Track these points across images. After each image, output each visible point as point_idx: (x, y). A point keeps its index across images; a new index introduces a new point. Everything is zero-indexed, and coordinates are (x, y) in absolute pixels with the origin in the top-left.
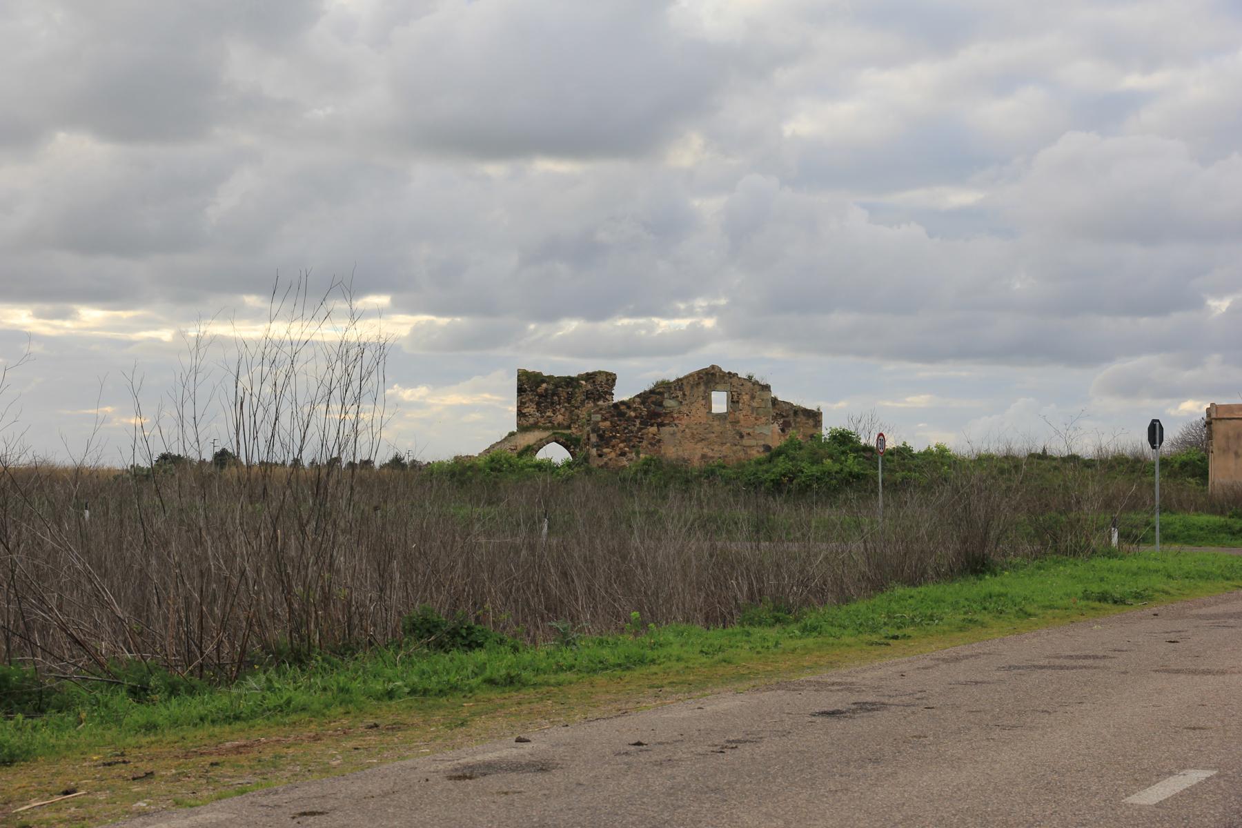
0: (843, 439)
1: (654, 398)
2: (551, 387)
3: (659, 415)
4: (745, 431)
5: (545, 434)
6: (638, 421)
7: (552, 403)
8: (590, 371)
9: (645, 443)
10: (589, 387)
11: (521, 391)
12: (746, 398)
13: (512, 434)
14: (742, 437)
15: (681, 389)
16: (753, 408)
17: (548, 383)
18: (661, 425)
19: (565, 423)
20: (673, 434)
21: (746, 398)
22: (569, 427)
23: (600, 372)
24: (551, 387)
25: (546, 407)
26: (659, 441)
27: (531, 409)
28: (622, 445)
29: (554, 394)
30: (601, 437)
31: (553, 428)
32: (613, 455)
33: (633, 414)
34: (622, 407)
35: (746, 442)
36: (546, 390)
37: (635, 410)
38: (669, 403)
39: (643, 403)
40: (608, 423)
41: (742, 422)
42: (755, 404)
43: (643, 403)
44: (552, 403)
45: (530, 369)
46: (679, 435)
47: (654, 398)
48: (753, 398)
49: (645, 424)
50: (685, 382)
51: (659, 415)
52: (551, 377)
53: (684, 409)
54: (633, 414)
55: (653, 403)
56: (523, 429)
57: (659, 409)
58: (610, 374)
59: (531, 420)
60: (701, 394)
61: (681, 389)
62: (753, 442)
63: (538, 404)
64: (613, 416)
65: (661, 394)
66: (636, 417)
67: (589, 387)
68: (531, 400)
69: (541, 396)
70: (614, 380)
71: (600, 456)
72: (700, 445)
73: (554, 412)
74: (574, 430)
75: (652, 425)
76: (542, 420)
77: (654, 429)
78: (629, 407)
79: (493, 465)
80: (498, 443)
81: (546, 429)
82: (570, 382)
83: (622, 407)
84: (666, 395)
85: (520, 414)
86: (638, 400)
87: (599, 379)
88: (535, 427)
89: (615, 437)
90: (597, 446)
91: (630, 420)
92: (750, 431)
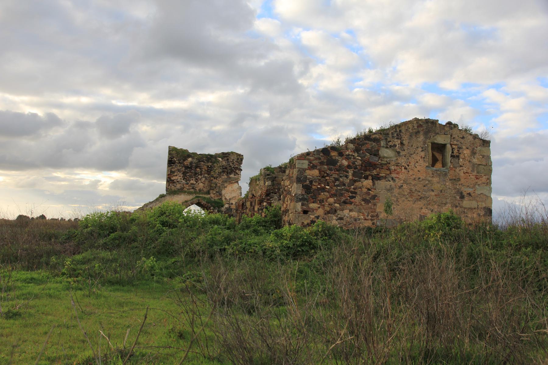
0: (70, 220)
1: (370, 145)
2: (195, 161)
3: (374, 166)
4: (466, 190)
5: (189, 197)
6: (351, 172)
7: (196, 174)
8: (226, 151)
9: (358, 199)
10: (224, 163)
11: (171, 162)
12: (467, 152)
13: (162, 196)
14: (462, 197)
15: (399, 137)
16: (474, 165)
17: (193, 158)
18: (376, 178)
19: (205, 190)
20: (390, 190)
21: (467, 152)
22: (208, 193)
23: (232, 153)
24: (195, 161)
25: (191, 177)
26: (374, 197)
27: (178, 177)
28: (331, 200)
29: (197, 167)
30: (307, 188)
31: (195, 192)
32: (321, 212)
33: (345, 163)
34: (334, 154)
35: (466, 203)
36: (191, 163)
37: (348, 158)
38: (386, 153)
39: (357, 150)
40: (316, 172)
41: (462, 181)
42: (475, 161)
43: (357, 150)
44: (196, 174)
45: (179, 147)
46: (396, 191)
47: (370, 145)
48: (473, 153)
49: (359, 175)
50: (403, 129)
51: (374, 166)
52: (195, 154)
53: (402, 161)
54: (345, 163)
55: (368, 150)
56: (171, 192)
57: (374, 159)
58: (240, 155)
59: (178, 186)
60: (420, 144)
61: (399, 137)
62: (474, 204)
63: (184, 174)
64: (322, 163)
65: (377, 141)
66: (349, 167)
67: (224, 163)
68: (179, 170)
69: (187, 167)
70: (242, 160)
71: (305, 212)
72: (420, 204)
73: (197, 181)
74: (212, 195)
75: (366, 178)
76: (187, 187)
77: (368, 183)
78: (341, 154)
79: (164, 218)
80: (151, 203)
81: (190, 193)
82: (210, 158)
83: (334, 154)
84: (383, 143)
85: (170, 181)
86: (351, 146)
87: (232, 157)
88: (181, 191)
89: (323, 189)
90: (302, 200)
91: (341, 169)
92: (470, 190)
